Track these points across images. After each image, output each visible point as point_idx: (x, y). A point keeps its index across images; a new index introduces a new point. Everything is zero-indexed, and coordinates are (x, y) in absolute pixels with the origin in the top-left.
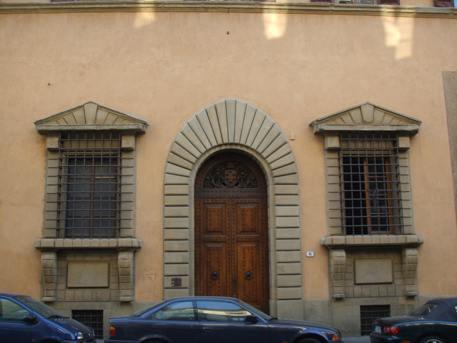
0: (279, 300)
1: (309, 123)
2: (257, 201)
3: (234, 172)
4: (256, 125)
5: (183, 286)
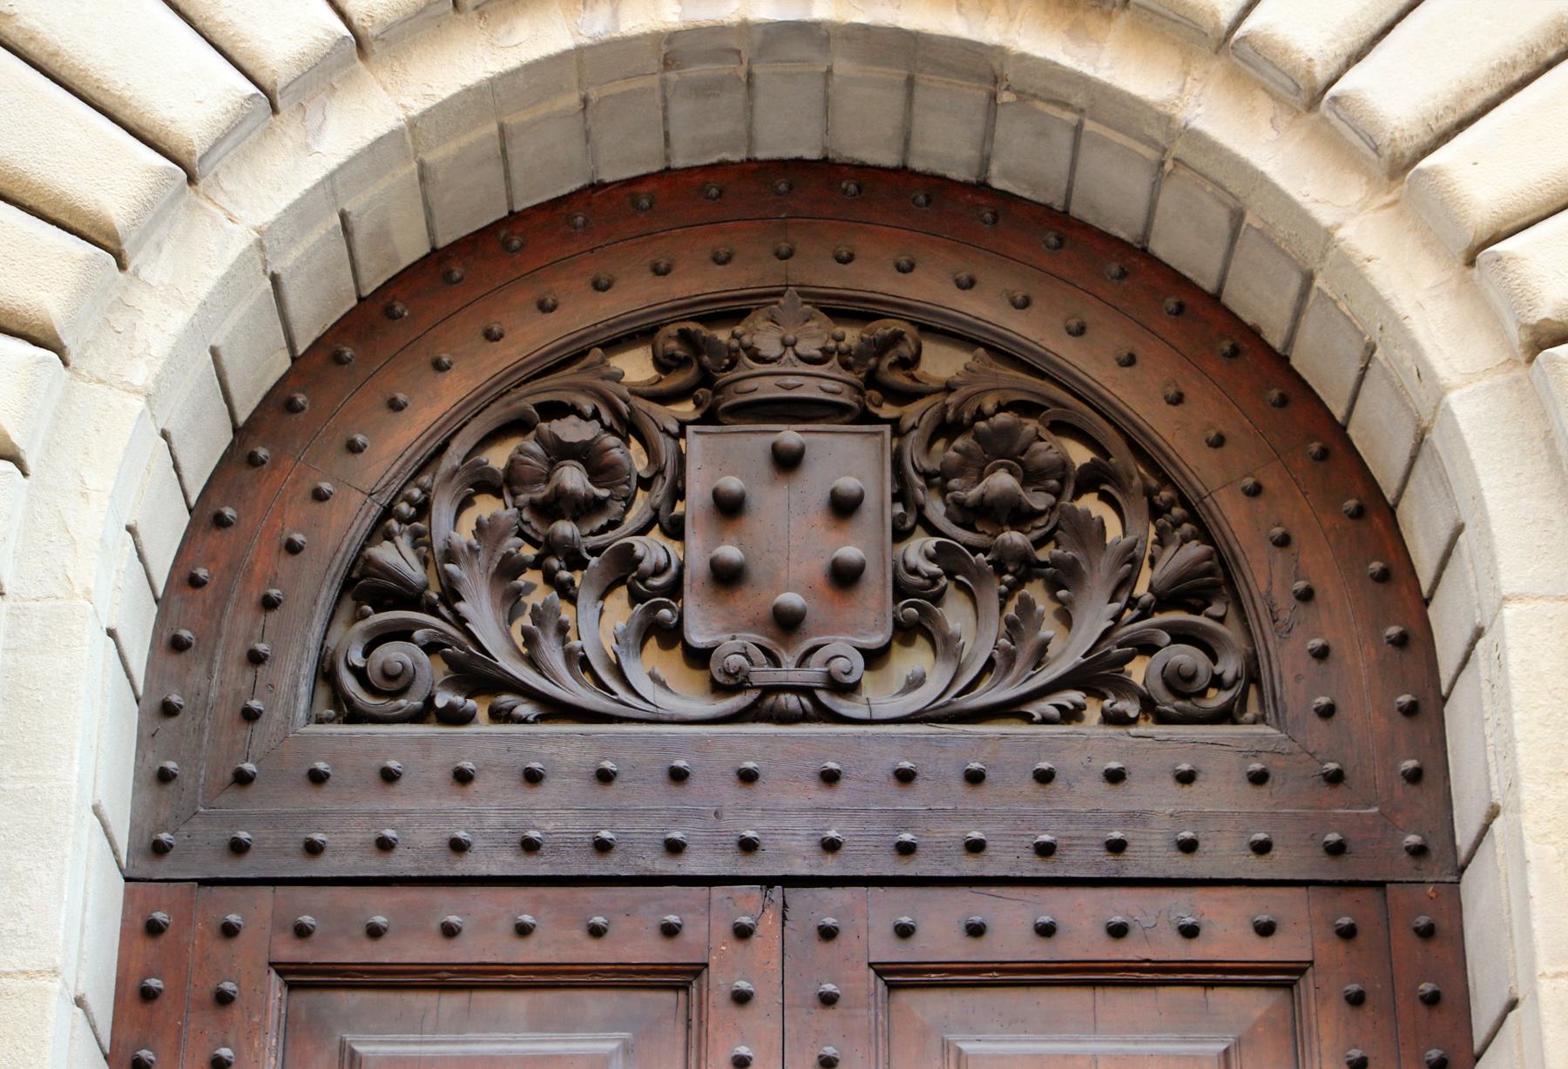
2: (1265, 930)
3: (847, 459)
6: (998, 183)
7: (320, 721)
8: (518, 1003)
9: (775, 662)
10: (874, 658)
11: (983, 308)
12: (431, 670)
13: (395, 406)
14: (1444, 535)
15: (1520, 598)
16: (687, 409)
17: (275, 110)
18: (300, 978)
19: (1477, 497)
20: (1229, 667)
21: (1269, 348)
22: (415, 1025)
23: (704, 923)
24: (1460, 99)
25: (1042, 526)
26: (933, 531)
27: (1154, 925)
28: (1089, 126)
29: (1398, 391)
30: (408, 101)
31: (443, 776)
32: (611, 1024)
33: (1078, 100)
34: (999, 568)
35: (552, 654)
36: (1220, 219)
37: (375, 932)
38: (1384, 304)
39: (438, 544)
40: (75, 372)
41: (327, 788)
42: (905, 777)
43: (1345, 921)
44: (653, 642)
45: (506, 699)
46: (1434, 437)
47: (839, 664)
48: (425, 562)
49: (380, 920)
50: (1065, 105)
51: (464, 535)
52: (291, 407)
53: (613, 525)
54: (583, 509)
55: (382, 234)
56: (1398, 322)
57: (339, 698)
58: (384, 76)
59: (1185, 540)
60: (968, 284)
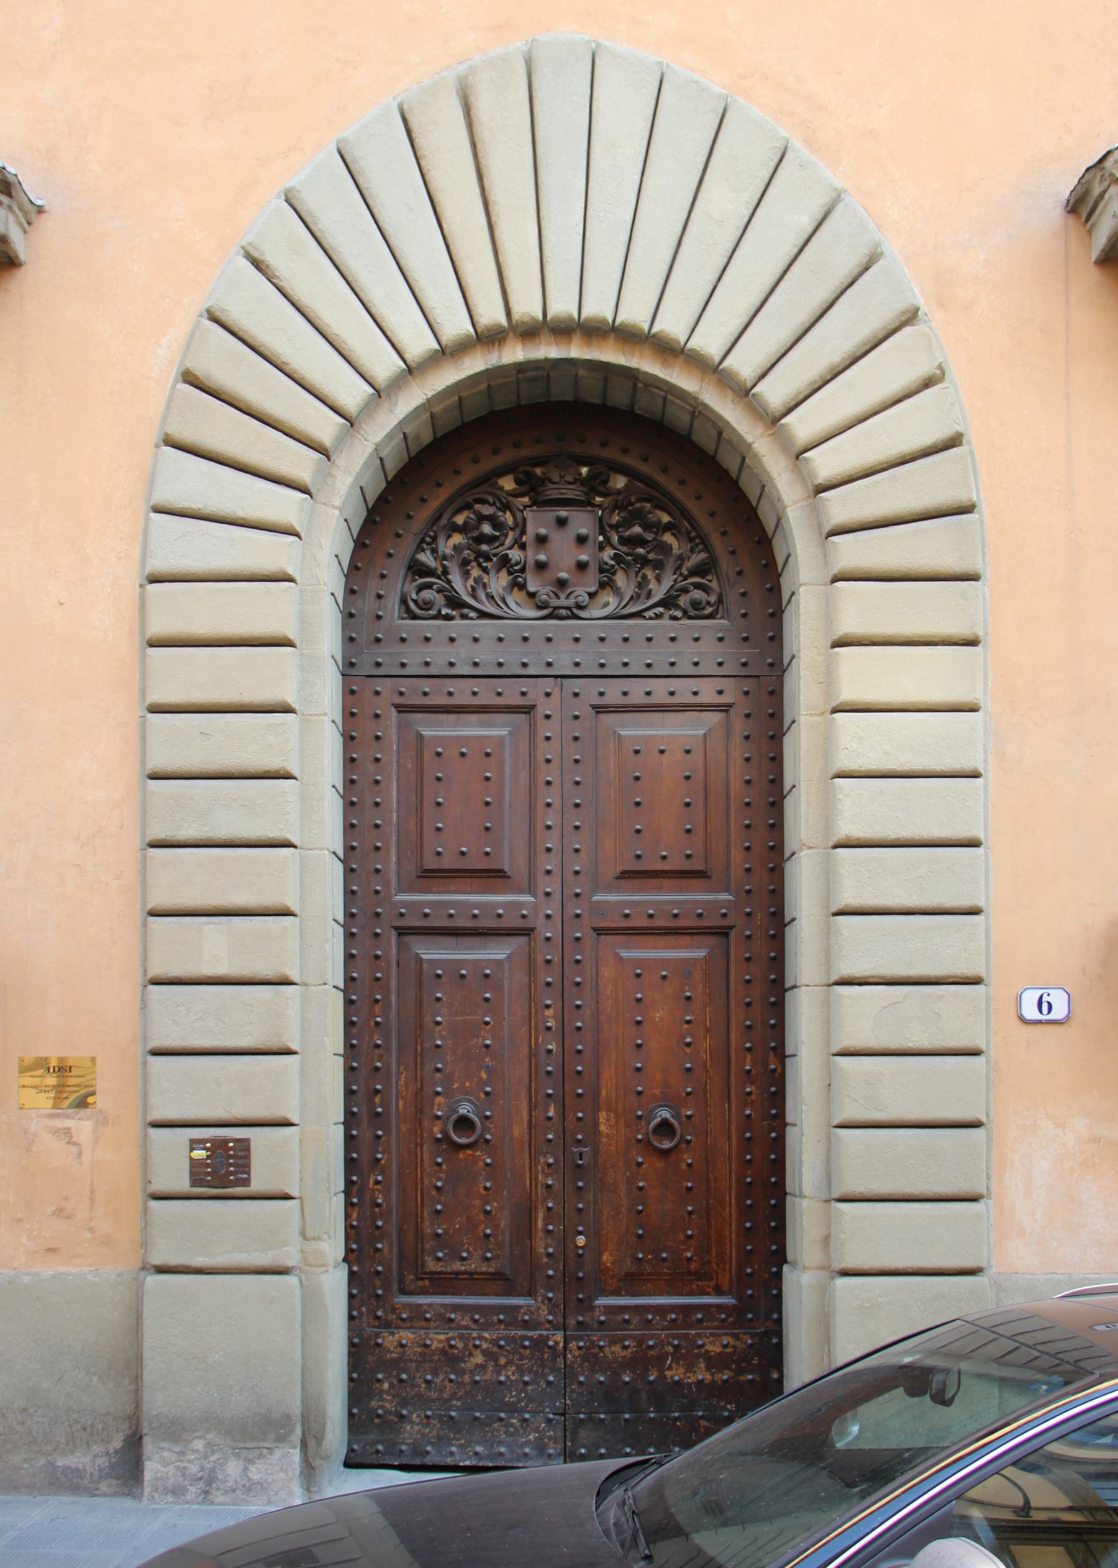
0: (845, 1273)
1: (1066, 186)
2: (720, 692)
3: (582, 522)
4: (724, 203)
5: (257, 1185)
6: (638, 412)
7: (403, 619)
8: (474, 717)
9: (558, 597)
10: (592, 595)
11: (630, 461)
12: (440, 599)
13: (423, 501)
14: (785, 556)
15: (805, 584)
16: (526, 500)
17: (380, 396)
18: (402, 709)
19: (795, 546)
20: (713, 599)
21: (731, 478)
22: (441, 725)
23: (535, 691)
24: (796, 396)
25: (650, 546)
26: (614, 548)
27: (684, 690)
28: (669, 397)
29: (772, 503)
30: (427, 392)
31: (446, 639)
32: (504, 725)
33: (665, 388)
34: (636, 560)
35: (483, 596)
36: (714, 433)
37: (425, 694)
38: (768, 473)
39: (440, 553)
40: (315, 501)
41: (407, 643)
42: (602, 639)
43: (746, 689)
44: (516, 589)
45: (466, 611)
46: (783, 521)
47: (580, 599)
48: (435, 559)
49: (427, 690)
50: (661, 389)
51: (449, 551)
52: (387, 501)
53: (502, 545)
54: (490, 540)
55: (417, 437)
56: (771, 480)
57: (408, 610)
58: (418, 381)
59: (700, 552)
60: (626, 451)
